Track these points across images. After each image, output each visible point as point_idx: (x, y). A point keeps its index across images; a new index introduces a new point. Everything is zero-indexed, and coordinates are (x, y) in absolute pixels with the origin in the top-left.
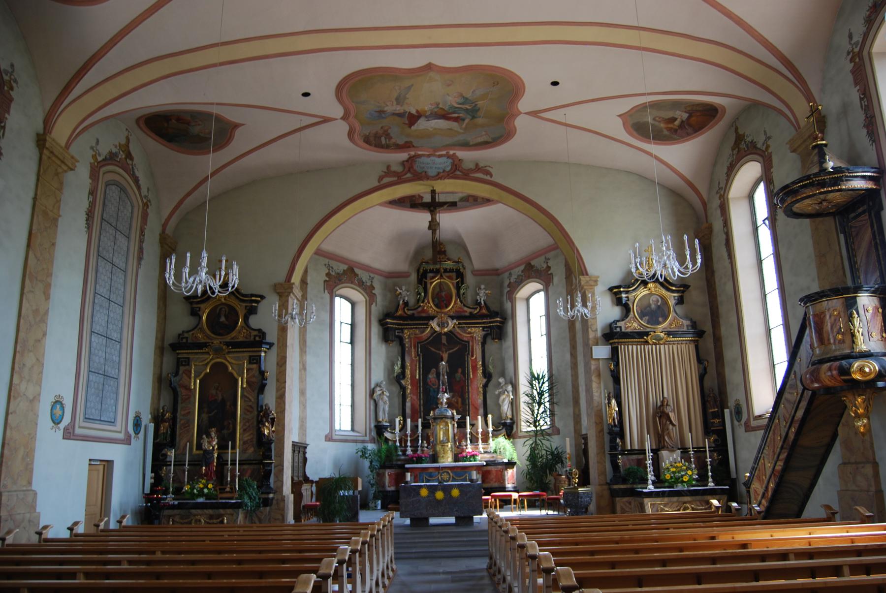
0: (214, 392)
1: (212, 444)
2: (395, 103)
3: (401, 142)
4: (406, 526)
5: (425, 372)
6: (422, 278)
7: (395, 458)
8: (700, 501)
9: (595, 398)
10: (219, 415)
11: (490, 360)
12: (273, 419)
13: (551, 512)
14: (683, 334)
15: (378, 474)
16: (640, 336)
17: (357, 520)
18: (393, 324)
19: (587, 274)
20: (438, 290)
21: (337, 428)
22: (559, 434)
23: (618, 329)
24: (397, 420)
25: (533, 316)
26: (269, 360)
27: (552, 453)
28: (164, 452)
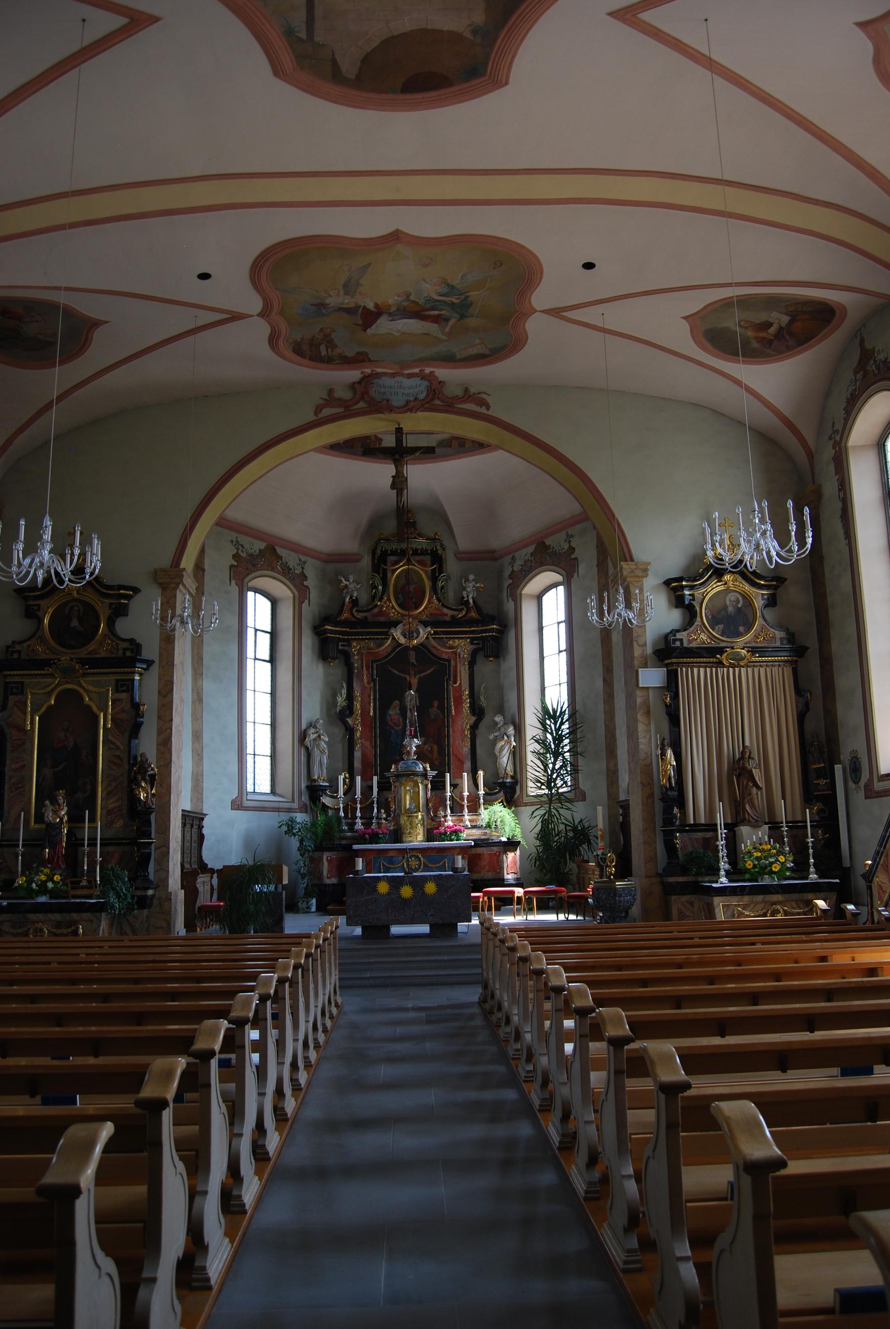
1: (59, 814)
2: (342, 292)
3: (350, 353)
4: (356, 937)
6: (380, 564)
7: (337, 835)
9: (642, 746)
12: (153, 777)
13: (572, 917)
14: (776, 651)
15: (312, 860)
16: (711, 654)
17: (282, 929)
18: (333, 633)
19: (632, 560)
21: (250, 788)
22: (584, 799)
23: (678, 644)
24: (341, 778)
25: (549, 617)
26: (146, 686)
27: (574, 829)
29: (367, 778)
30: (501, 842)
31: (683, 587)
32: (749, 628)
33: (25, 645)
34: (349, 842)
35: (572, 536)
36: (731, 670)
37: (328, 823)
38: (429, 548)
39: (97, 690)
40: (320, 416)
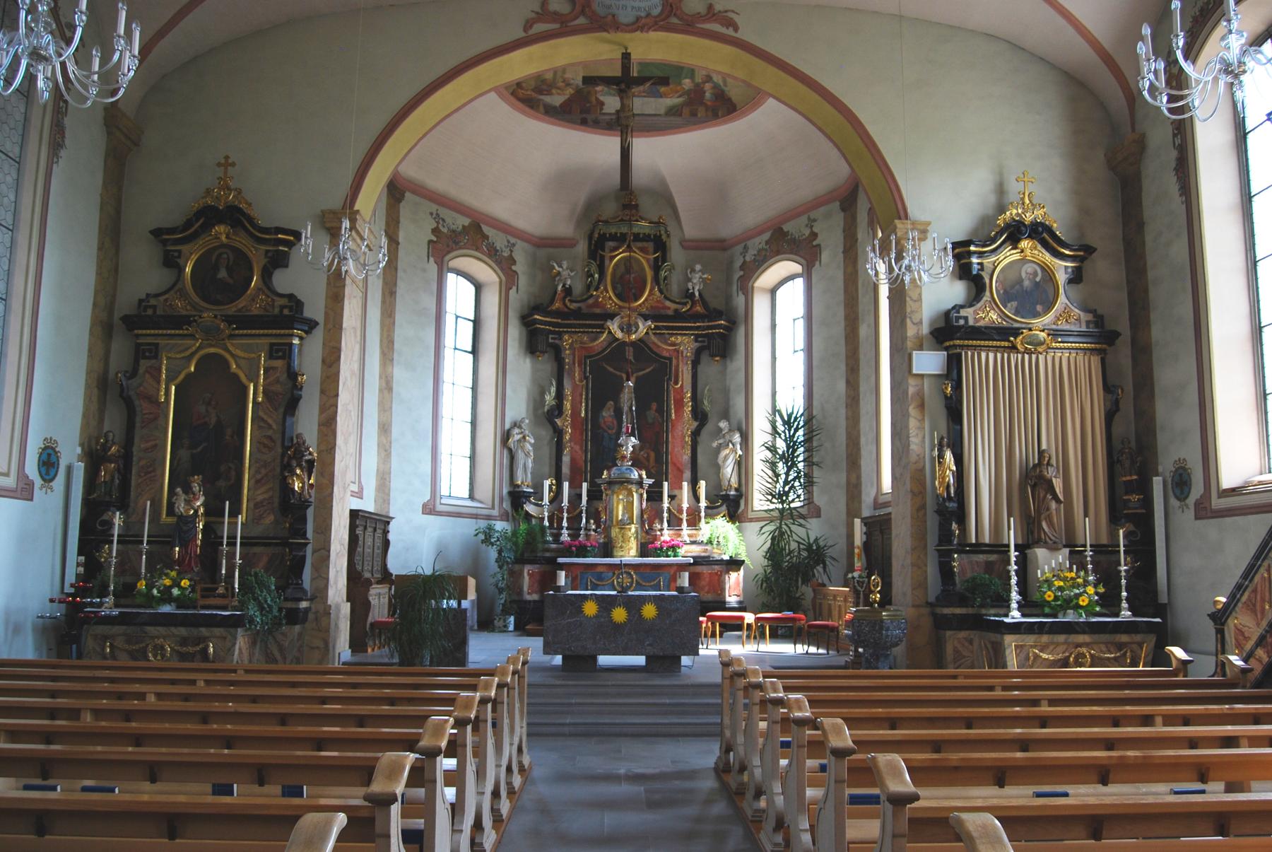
0: (202, 409)
4: (555, 668)
5: (597, 405)
6: (597, 248)
7: (540, 546)
8: (1106, 643)
9: (913, 447)
10: (209, 454)
11: (705, 391)
12: (311, 463)
13: (813, 650)
15: (512, 573)
16: (1003, 335)
17: (462, 661)
18: (546, 325)
19: (906, 217)
20: (622, 269)
21: (444, 491)
22: (819, 516)
23: (962, 322)
24: (547, 483)
27: (809, 548)
28: (105, 517)
29: (575, 486)
30: (722, 560)
31: (970, 254)
32: (1048, 308)
33: (162, 298)
34: (553, 554)
35: (815, 220)
36: (1027, 356)
37: (530, 532)
38: (653, 232)
39: (246, 355)
40: (531, 32)
